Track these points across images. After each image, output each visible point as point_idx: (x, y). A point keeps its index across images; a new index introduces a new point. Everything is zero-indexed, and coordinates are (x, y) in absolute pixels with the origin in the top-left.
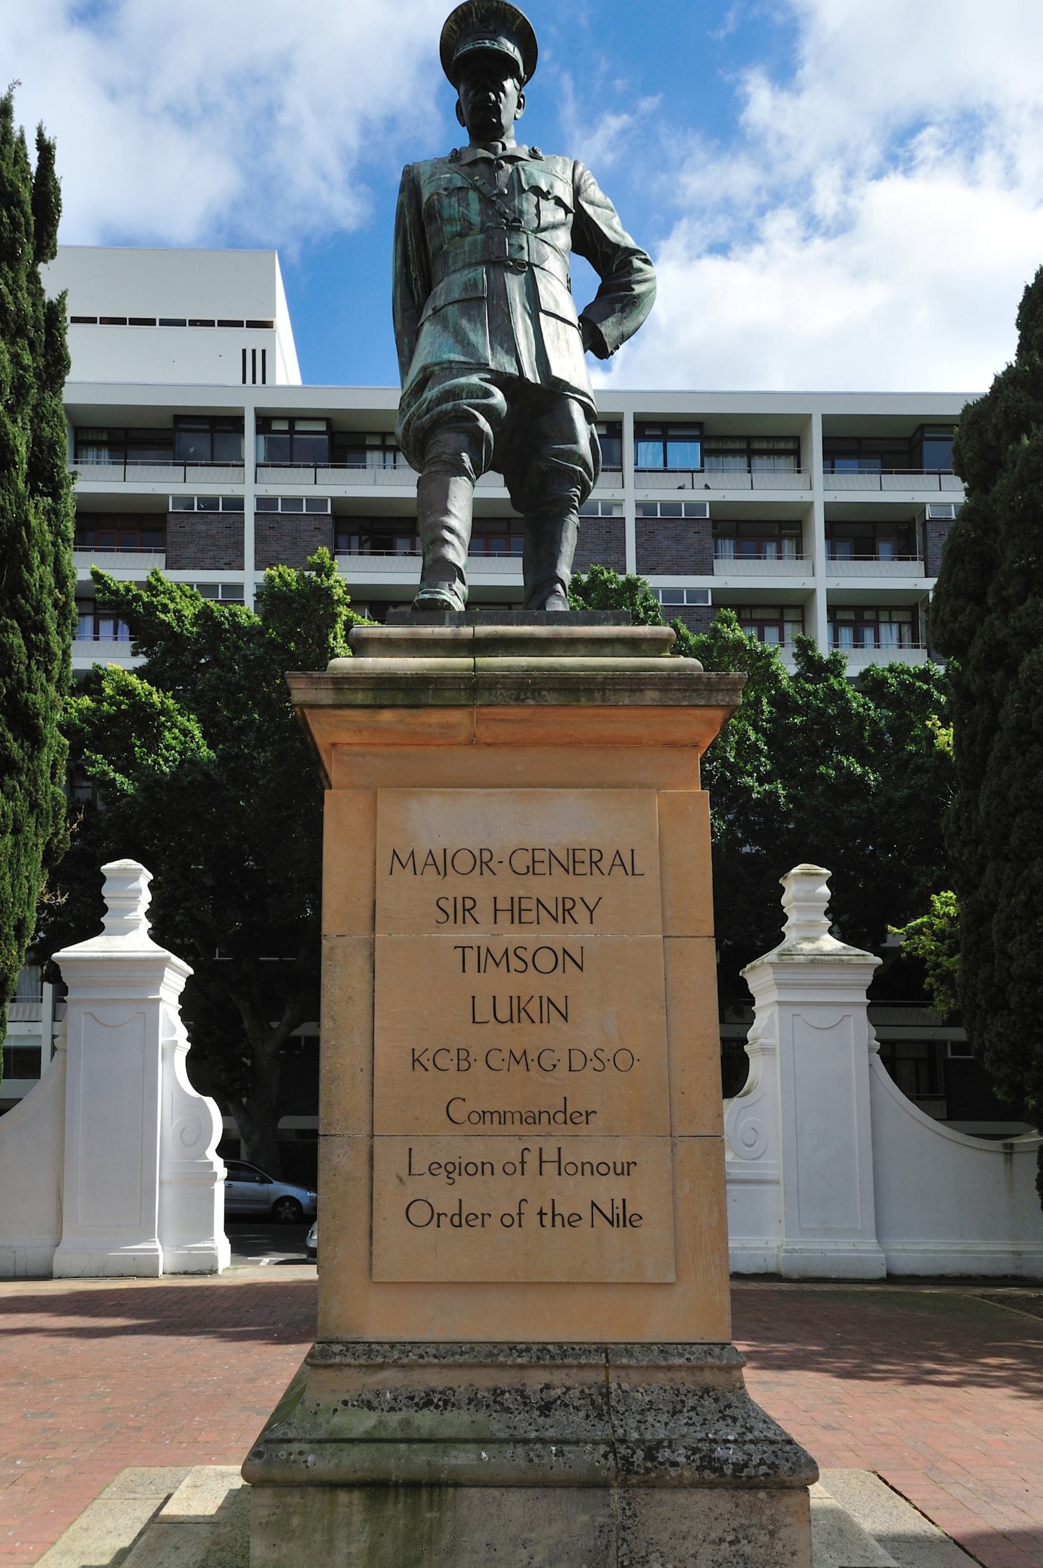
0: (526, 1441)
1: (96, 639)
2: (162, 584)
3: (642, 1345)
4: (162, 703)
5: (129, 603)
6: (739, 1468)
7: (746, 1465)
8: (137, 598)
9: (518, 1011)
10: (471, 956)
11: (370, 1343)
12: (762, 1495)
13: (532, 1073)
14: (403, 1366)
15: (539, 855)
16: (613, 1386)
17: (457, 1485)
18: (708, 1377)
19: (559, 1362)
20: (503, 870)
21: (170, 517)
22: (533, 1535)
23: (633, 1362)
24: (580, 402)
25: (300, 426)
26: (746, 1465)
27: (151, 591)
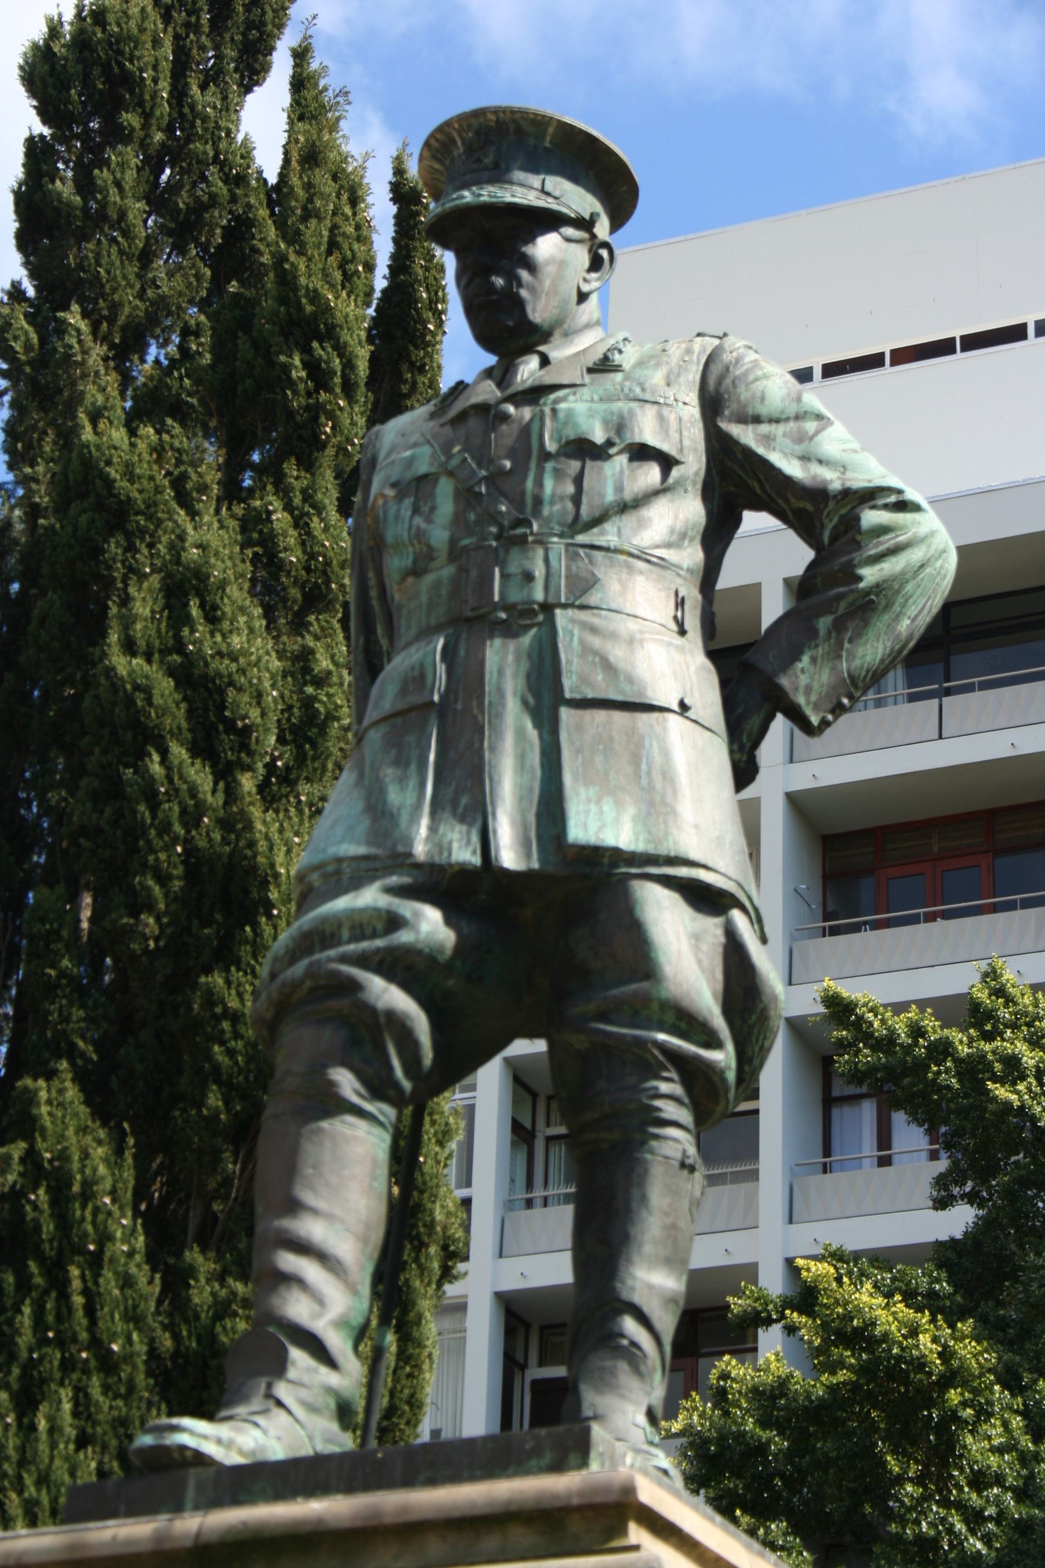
1: (885, 1162)
2: (1009, 1000)
5: (921, 1066)
8: (942, 1050)
24: (667, 882)
27: (978, 1025)
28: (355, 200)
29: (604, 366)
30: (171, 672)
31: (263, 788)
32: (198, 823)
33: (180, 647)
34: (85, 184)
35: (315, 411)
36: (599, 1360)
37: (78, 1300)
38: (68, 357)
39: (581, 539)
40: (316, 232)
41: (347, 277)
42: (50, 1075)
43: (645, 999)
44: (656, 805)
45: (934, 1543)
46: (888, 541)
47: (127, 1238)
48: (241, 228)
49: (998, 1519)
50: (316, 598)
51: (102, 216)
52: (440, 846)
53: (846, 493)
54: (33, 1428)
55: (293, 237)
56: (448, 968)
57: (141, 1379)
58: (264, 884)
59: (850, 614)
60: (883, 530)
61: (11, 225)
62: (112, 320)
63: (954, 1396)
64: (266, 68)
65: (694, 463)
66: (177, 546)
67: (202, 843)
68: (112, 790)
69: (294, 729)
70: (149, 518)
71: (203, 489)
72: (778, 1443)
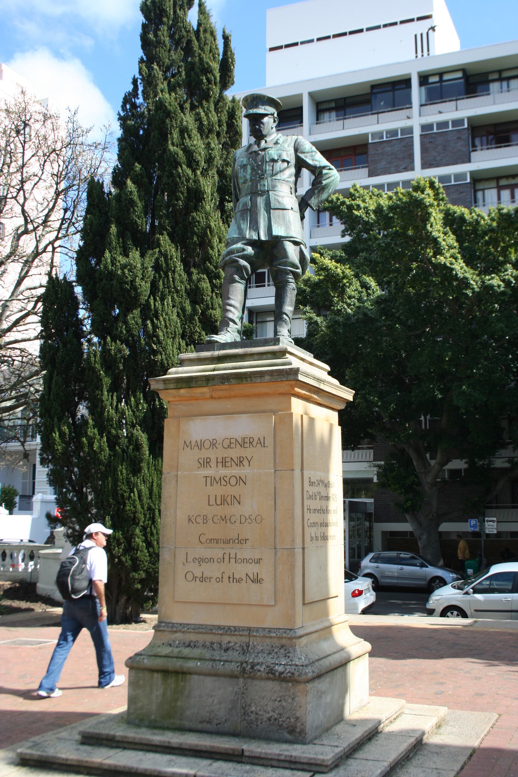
0: (215, 660)
1: (331, 225)
2: (358, 192)
3: (263, 628)
4: (343, 272)
5: (339, 207)
6: (281, 673)
7: (283, 673)
9: (224, 501)
10: (209, 480)
11: (173, 624)
12: (290, 684)
13: (228, 524)
14: (183, 632)
15: (232, 441)
16: (251, 643)
17: (190, 674)
18: (284, 641)
19: (233, 633)
20: (220, 447)
21: (369, 146)
22: (214, 693)
23: (258, 634)
24: (290, 241)
25: (446, 77)
26: (283, 673)
27: (351, 197)
28: (215, 40)
29: (276, 143)
30: (182, 149)
31: (201, 173)
32: (189, 181)
33: (183, 144)
34: (156, 35)
35: (209, 89)
36: (280, 322)
37: (171, 279)
38: (154, 76)
39: (274, 178)
40: (207, 48)
41: (214, 58)
42: (162, 234)
43: (286, 262)
44: (287, 228)
45: (341, 310)
46: (327, 176)
47: (180, 267)
48: (189, 42)
49: (354, 305)
50: (210, 131)
51: (160, 43)
52: (251, 236)
53: (320, 167)
54: (164, 304)
55: (202, 49)
56: (253, 257)
57: (184, 294)
58: (203, 194)
59: (321, 190)
60: (326, 174)
61: (139, 43)
62: (163, 66)
63: (345, 281)
64: (193, 4)
65: (293, 162)
66: (181, 122)
67: (190, 186)
68: (171, 175)
69: (207, 160)
70: (175, 114)
71: (186, 108)
72: (308, 290)
